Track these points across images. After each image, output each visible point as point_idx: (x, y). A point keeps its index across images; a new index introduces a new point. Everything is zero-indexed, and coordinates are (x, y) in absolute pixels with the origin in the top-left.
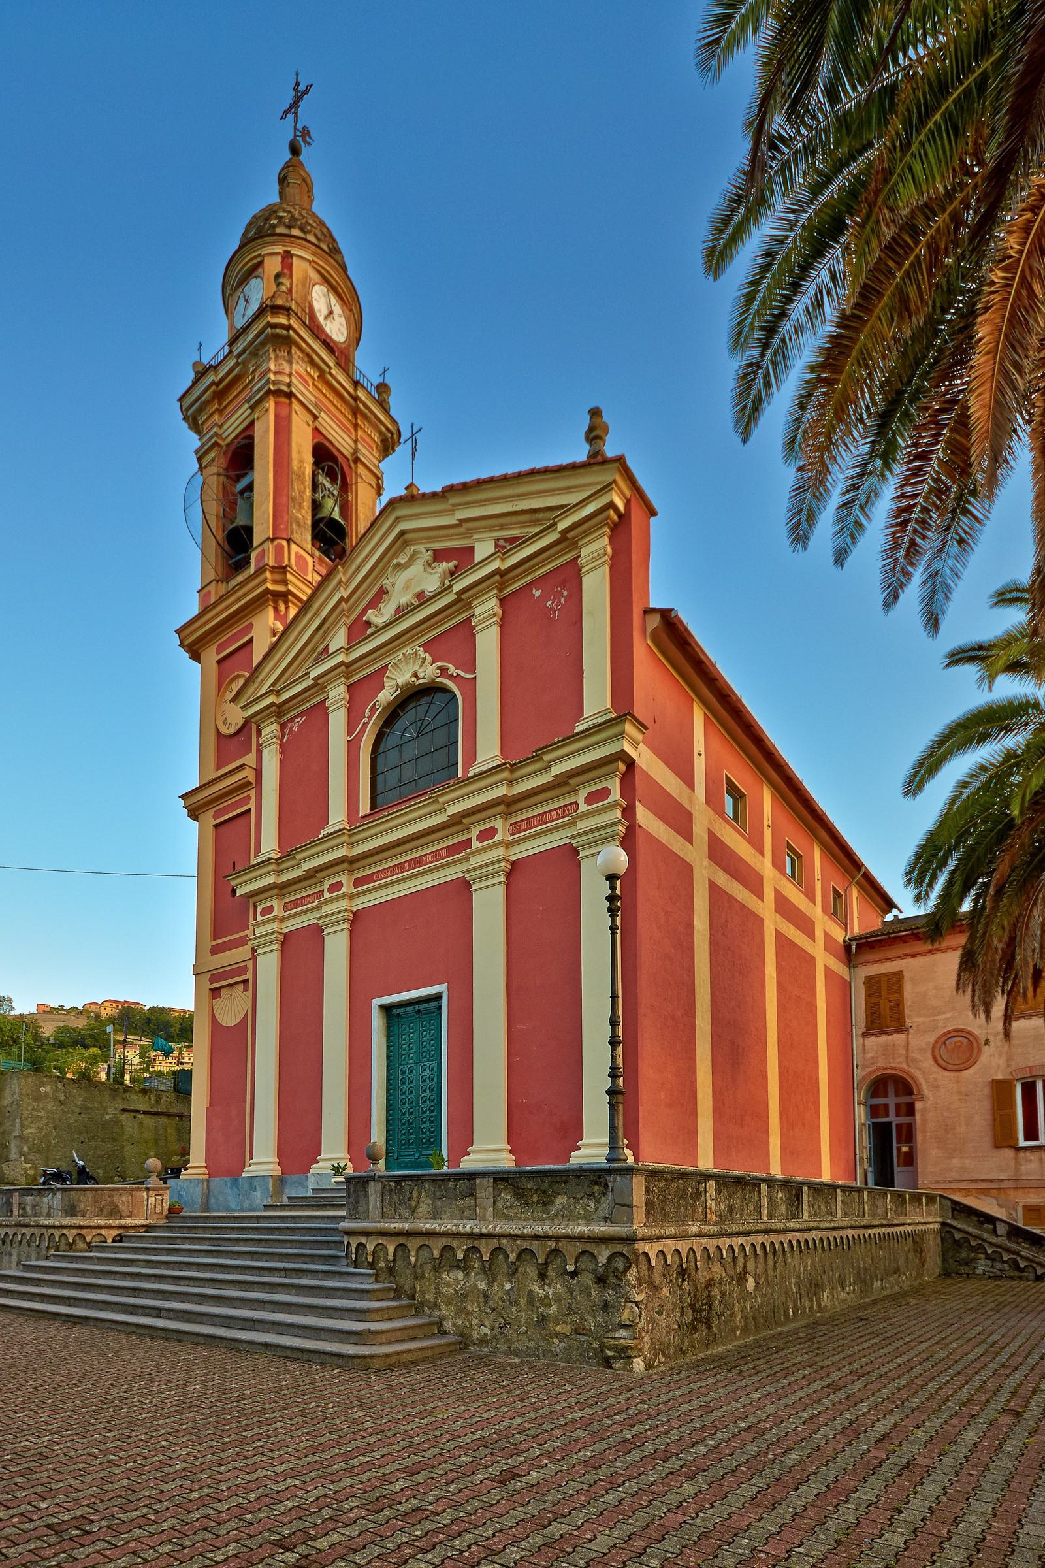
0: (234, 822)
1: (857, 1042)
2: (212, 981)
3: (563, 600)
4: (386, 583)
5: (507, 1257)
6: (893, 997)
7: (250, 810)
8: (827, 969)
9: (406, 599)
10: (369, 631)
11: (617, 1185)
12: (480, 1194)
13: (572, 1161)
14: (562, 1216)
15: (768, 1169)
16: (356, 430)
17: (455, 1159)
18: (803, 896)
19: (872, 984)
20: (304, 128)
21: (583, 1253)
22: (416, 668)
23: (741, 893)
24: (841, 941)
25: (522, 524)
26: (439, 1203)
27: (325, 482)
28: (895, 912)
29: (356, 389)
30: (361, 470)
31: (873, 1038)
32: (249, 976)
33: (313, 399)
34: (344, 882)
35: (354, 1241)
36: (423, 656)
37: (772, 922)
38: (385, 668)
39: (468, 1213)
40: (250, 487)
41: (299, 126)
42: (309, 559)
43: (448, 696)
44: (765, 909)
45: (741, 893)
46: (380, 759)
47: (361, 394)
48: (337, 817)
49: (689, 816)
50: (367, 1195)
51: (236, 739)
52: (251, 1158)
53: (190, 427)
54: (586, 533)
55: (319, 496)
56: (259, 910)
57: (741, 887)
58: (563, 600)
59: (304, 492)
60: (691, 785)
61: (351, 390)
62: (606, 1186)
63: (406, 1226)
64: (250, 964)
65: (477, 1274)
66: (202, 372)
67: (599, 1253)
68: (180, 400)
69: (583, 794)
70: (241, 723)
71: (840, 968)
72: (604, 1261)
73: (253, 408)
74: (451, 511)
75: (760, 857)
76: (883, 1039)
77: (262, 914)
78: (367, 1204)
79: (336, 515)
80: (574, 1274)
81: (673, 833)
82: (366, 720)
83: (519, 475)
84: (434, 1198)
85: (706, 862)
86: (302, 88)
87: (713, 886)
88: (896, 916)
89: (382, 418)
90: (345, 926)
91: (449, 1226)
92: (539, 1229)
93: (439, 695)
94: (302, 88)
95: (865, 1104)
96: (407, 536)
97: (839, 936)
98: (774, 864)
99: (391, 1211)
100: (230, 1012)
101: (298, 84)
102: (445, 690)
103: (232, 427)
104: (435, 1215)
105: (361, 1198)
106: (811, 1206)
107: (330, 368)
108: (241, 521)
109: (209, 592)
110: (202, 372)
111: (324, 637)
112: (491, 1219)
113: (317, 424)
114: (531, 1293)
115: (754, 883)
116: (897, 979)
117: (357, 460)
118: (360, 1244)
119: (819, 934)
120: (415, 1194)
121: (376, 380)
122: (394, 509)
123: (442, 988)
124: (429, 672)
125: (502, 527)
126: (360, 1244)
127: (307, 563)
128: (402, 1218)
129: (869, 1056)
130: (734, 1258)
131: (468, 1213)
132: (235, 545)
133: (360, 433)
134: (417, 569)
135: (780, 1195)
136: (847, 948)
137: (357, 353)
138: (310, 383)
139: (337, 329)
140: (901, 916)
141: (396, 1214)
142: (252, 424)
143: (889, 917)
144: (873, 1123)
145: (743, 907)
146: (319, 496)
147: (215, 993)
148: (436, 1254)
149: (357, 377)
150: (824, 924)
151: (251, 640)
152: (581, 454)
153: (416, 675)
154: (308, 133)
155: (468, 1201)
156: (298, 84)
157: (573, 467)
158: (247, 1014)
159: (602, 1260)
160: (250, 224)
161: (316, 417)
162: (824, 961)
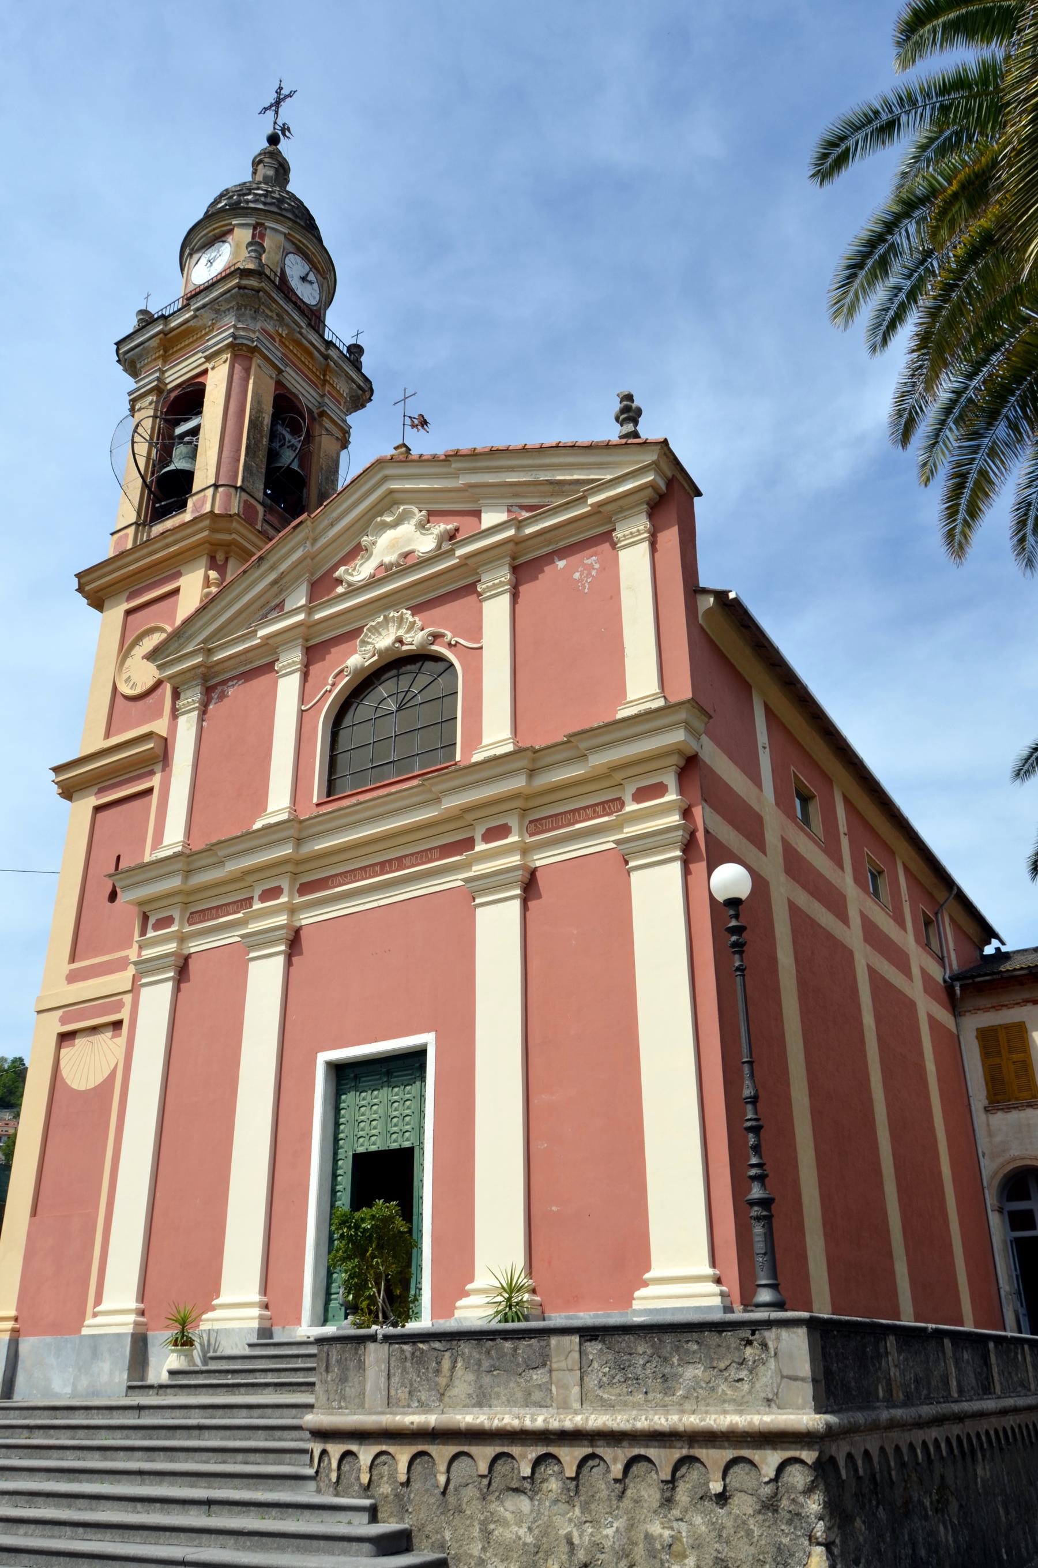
0: (690, 898)
1: (980, 1118)
2: (63, 1021)
3: (594, 573)
4: (365, 540)
5: (608, 1470)
6: (1016, 1057)
7: (150, 791)
8: (932, 1020)
9: (390, 558)
10: (340, 590)
11: (783, 1346)
12: (557, 1362)
13: (636, 1305)
14: (693, 1398)
15: (717, 1306)
16: (324, 385)
17: (444, 1305)
18: (891, 921)
19: (987, 1037)
20: (284, 124)
21: (378, 1455)
22: (401, 632)
23: (825, 918)
24: (941, 981)
25: (543, 495)
26: (487, 1380)
27: (284, 432)
28: (995, 943)
29: (327, 349)
30: (328, 424)
31: (1000, 1115)
32: (124, 1015)
33: (279, 354)
34: (285, 885)
35: (336, 1450)
36: (411, 619)
37: (863, 957)
38: (360, 630)
39: (537, 1396)
40: (195, 431)
41: (280, 122)
42: (260, 509)
43: (441, 666)
44: (853, 937)
45: (825, 918)
46: (343, 734)
47: (332, 353)
48: (278, 802)
49: (759, 819)
50: (361, 1366)
51: (140, 704)
52: (98, 1301)
53: (125, 370)
54: (622, 510)
55: (276, 445)
56: (152, 921)
57: (824, 910)
58: (594, 573)
59: (260, 441)
60: (758, 784)
61: (322, 349)
62: (764, 1345)
63: (431, 1420)
64: (127, 999)
65: (556, 1501)
66: (147, 320)
67: (764, 1460)
68: (118, 344)
69: (630, 790)
70: (150, 683)
71: (945, 1017)
72: (772, 1474)
73: (208, 359)
74: (455, 475)
75: (840, 872)
76: (1014, 1116)
77: (155, 928)
78: (363, 1383)
79: (295, 466)
80: (722, 1498)
81: (745, 841)
82: (329, 687)
83: (541, 450)
84: (478, 1372)
85: (783, 877)
86: (285, 92)
87: (794, 909)
88: (998, 949)
89: (354, 376)
90: (283, 948)
91: (507, 1418)
92: (662, 1421)
93: (429, 665)
94: (285, 92)
95: (1001, 1211)
96: (396, 496)
97: (937, 973)
98: (856, 880)
99: (402, 1394)
100: (87, 1065)
101: (281, 88)
102: (438, 658)
103: (177, 374)
104: (481, 1400)
105: (351, 1374)
106: (1001, 1373)
107: (301, 327)
108: (178, 463)
109: (127, 535)
110: (147, 320)
111: (281, 591)
112: (576, 1405)
113: (281, 377)
114: (648, 1536)
115: (837, 905)
116: (1019, 1033)
117: (323, 414)
118: (348, 1453)
119: (916, 971)
120: (446, 1364)
121: (349, 341)
122: (382, 468)
123: (427, 1039)
124: (415, 639)
125: (516, 495)
126: (348, 1453)
127: (257, 512)
128: (424, 1407)
129: (997, 1139)
130: (930, 1461)
131: (537, 1396)
132: (167, 490)
133: (327, 388)
134: (407, 529)
135: (966, 1356)
136: (949, 989)
137: (328, 312)
138: (277, 340)
139: (309, 294)
140: (1004, 949)
141: (413, 1400)
142: (205, 372)
143: (989, 950)
144: (1017, 1241)
145: (830, 936)
146: (276, 445)
147: (66, 1037)
148: (483, 1468)
149: (328, 336)
150: (919, 959)
151: (176, 591)
152: (612, 432)
153: (400, 640)
154: (289, 130)
155: (538, 1376)
156: (281, 88)
157: (608, 446)
158: (114, 1072)
159: (769, 1471)
160: (222, 195)
161: (280, 372)
162: (928, 1008)
